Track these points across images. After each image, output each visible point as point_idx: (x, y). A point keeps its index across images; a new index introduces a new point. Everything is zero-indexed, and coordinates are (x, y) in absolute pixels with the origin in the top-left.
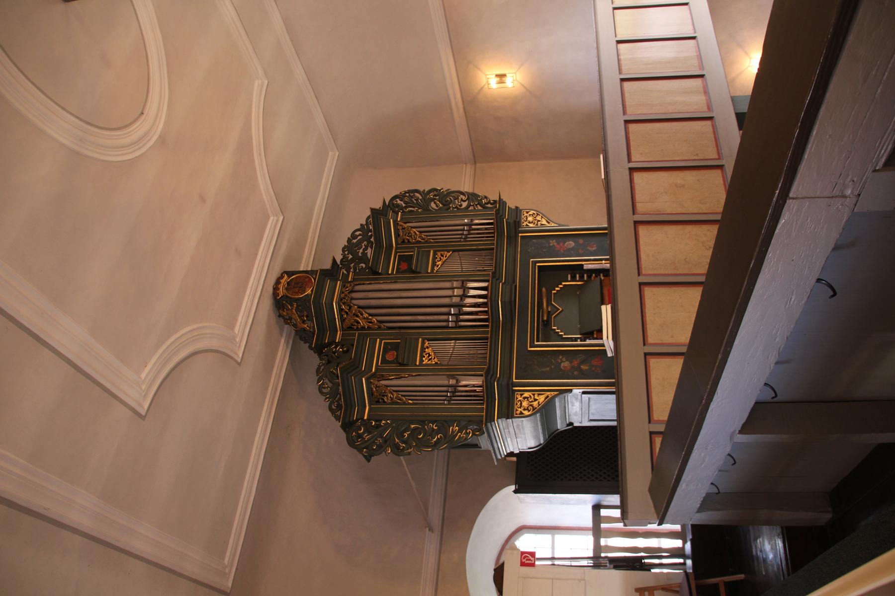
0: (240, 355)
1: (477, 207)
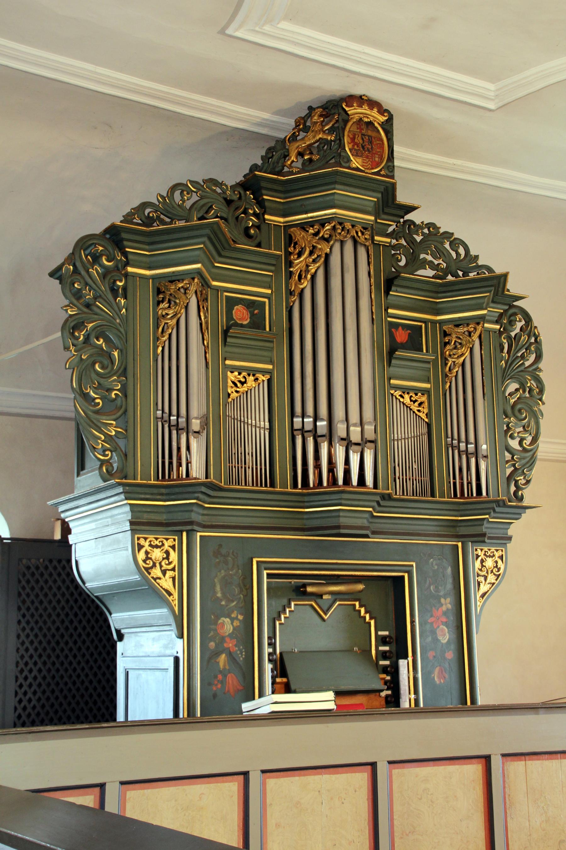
0: (238, 34)
1: (509, 467)
